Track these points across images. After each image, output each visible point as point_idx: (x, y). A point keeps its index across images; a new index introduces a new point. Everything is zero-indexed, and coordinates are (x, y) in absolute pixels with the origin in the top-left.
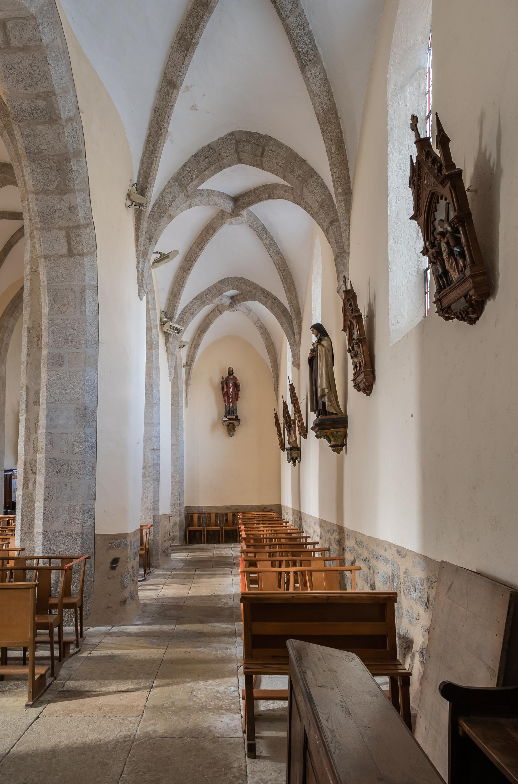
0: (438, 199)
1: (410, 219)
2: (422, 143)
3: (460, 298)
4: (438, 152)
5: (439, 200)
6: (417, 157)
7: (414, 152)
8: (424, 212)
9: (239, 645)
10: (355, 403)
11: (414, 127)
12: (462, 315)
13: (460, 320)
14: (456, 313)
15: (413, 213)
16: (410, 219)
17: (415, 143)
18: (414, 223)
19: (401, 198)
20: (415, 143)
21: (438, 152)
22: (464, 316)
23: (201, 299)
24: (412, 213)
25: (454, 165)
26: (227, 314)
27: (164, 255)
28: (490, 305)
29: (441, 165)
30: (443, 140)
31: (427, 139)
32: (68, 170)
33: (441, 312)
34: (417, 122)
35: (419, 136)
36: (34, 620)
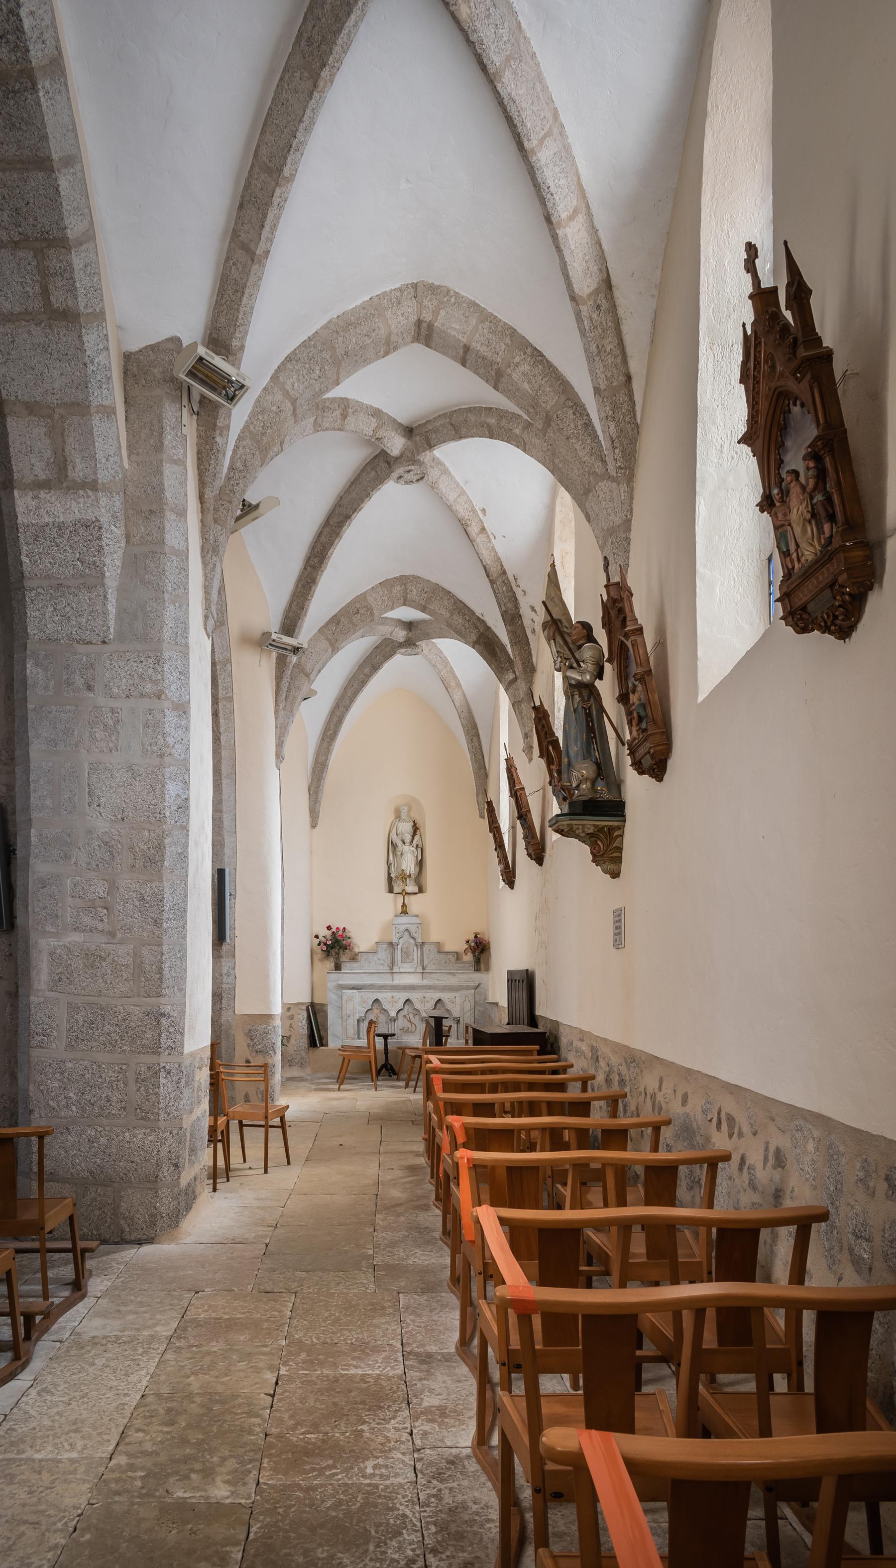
0: (788, 405)
1: (739, 442)
2: (763, 298)
3: (822, 590)
4: (788, 315)
5: (791, 406)
6: (753, 324)
7: (748, 316)
8: (765, 434)
9: (453, 1309)
10: (636, 786)
11: (750, 266)
12: (826, 623)
13: (823, 633)
14: (816, 618)
15: (745, 430)
16: (739, 442)
17: (751, 297)
18: (746, 449)
19: (724, 405)
20: (751, 297)
21: (788, 315)
22: (829, 624)
23: (339, 627)
24: (742, 429)
25: (819, 340)
26: (399, 662)
27: (250, 505)
28: (874, 602)
29: (795, 340)
30: (799, 292)
31: (774, 291)
32: (79, 682)
33: (790, 619)
34: (757, 257)
35: (759, 282)
36: (37, 1314)
